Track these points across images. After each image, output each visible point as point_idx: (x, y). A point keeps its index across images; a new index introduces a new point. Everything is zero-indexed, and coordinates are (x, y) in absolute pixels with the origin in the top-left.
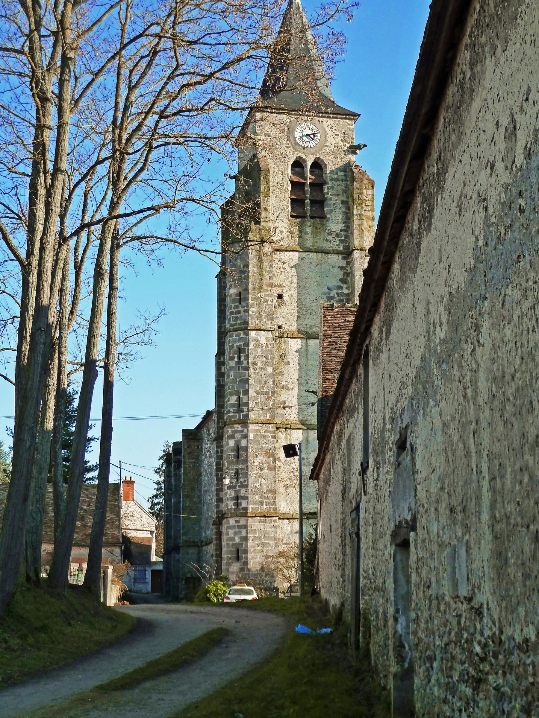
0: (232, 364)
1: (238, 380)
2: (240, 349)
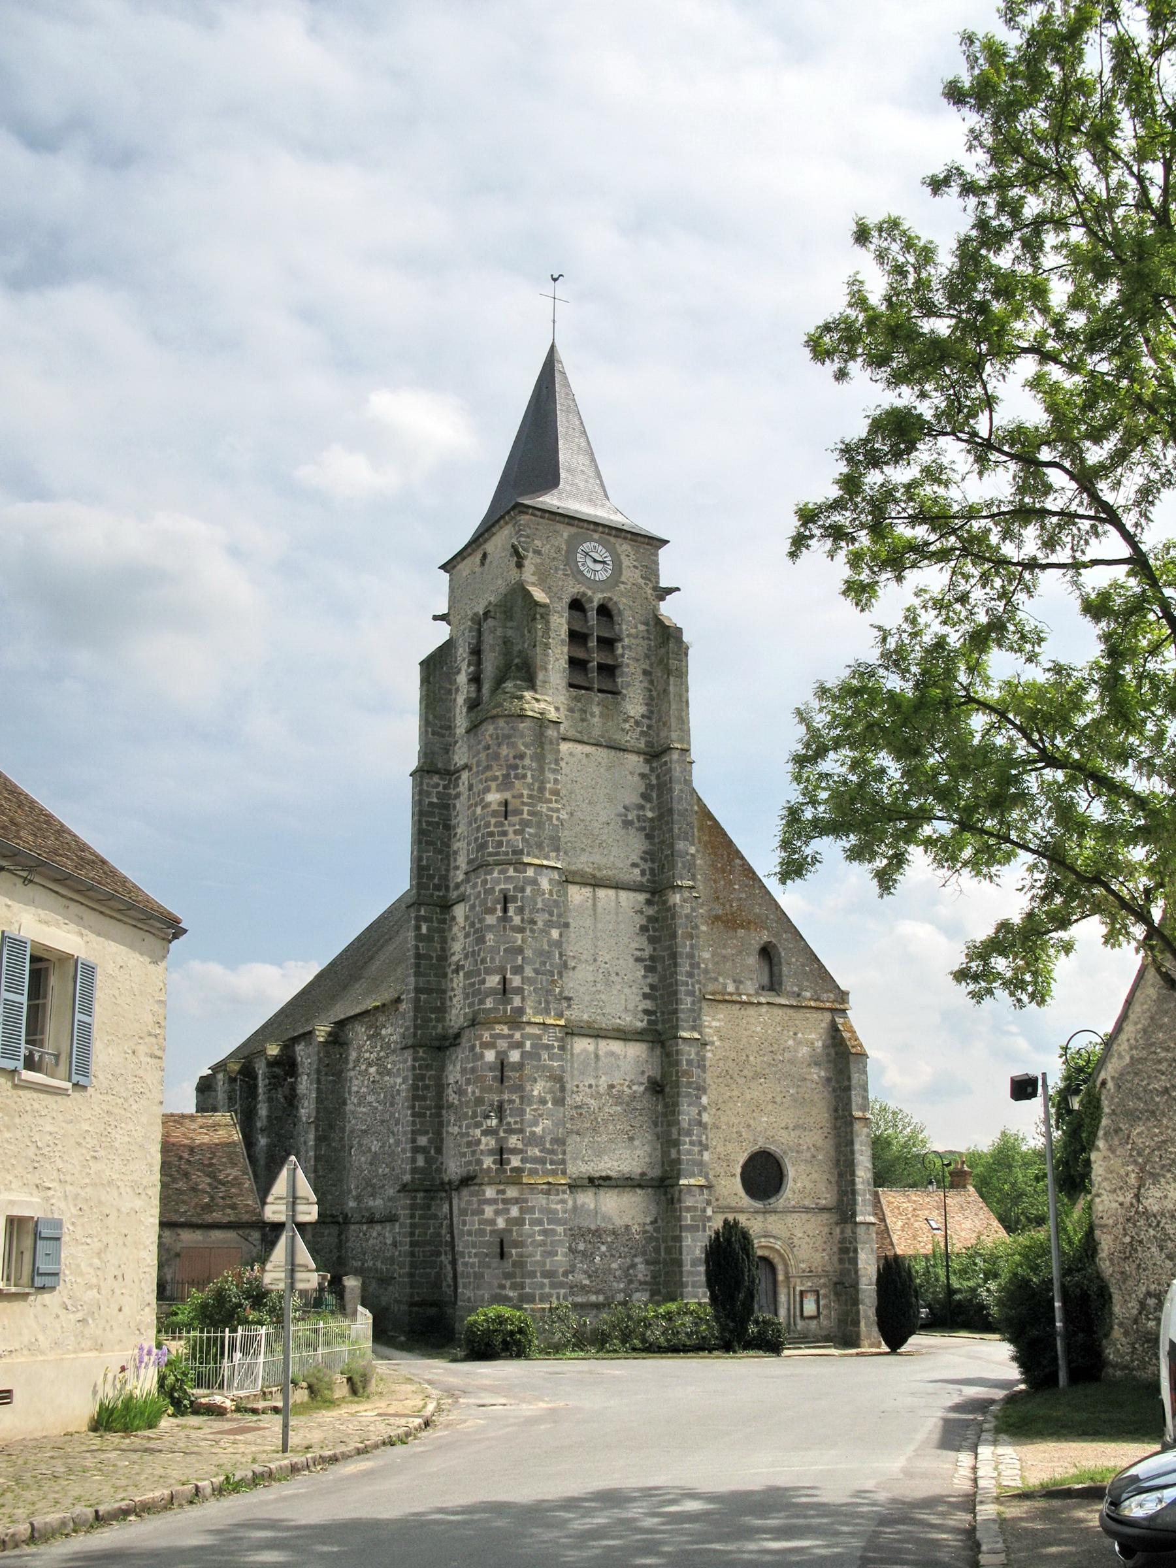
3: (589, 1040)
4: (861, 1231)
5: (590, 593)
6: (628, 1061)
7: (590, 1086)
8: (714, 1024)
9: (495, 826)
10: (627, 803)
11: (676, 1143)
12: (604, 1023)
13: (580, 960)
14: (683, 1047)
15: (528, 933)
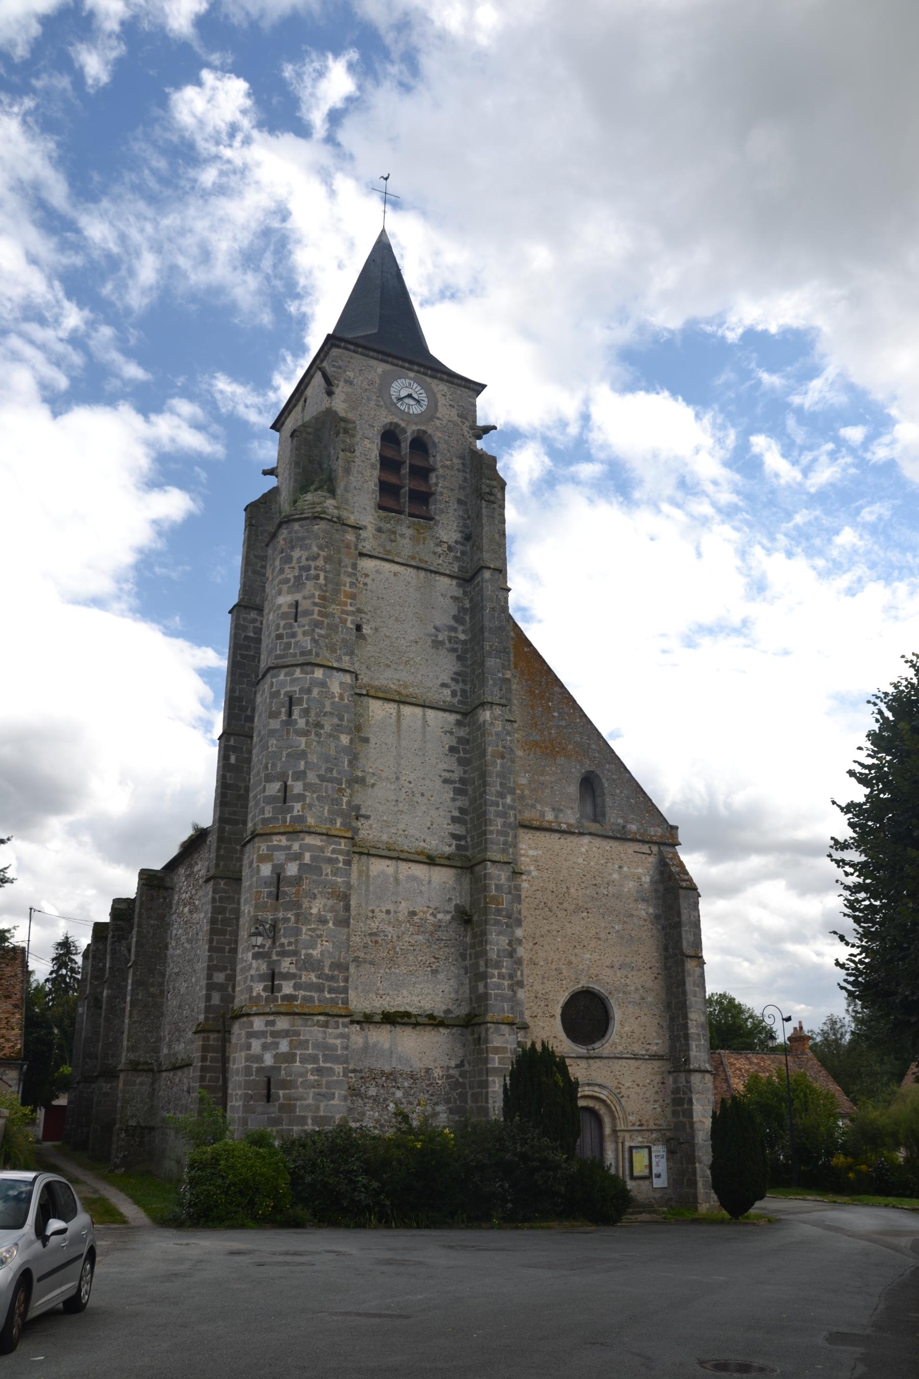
0: (275, 724)
1: (284, 754)
2: (291, 698)
3: (388, 862)
4: (696, 1078)
5: (403, 424)
6: (432, 890)
7: (388, 912)
8: (531, 852)
9: (284, 628)
10: (438, 623)
11: (483, 976)
12: (405, 844)
13: (380, 778)
14: (491, 869)
15: (313, 736)
